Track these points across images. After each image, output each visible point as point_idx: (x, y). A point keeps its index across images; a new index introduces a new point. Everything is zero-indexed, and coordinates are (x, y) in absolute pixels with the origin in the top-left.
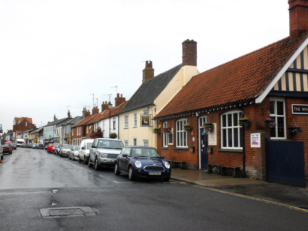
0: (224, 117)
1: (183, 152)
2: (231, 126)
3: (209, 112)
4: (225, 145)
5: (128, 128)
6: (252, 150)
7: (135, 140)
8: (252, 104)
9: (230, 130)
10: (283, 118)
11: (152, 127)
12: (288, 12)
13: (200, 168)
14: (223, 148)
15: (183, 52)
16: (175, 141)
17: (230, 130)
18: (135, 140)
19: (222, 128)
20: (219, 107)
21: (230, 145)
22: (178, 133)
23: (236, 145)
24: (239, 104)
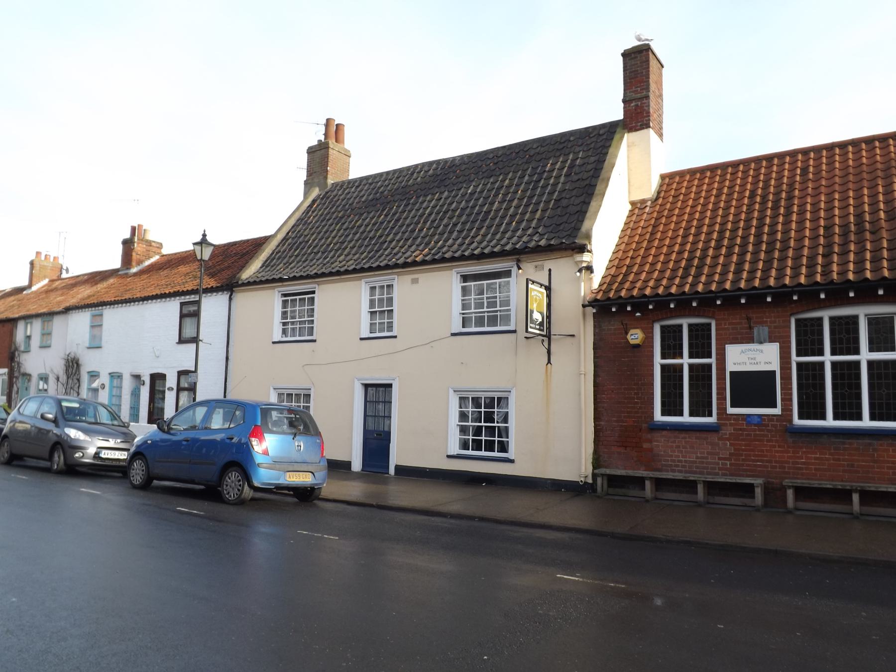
16: (787, 399)
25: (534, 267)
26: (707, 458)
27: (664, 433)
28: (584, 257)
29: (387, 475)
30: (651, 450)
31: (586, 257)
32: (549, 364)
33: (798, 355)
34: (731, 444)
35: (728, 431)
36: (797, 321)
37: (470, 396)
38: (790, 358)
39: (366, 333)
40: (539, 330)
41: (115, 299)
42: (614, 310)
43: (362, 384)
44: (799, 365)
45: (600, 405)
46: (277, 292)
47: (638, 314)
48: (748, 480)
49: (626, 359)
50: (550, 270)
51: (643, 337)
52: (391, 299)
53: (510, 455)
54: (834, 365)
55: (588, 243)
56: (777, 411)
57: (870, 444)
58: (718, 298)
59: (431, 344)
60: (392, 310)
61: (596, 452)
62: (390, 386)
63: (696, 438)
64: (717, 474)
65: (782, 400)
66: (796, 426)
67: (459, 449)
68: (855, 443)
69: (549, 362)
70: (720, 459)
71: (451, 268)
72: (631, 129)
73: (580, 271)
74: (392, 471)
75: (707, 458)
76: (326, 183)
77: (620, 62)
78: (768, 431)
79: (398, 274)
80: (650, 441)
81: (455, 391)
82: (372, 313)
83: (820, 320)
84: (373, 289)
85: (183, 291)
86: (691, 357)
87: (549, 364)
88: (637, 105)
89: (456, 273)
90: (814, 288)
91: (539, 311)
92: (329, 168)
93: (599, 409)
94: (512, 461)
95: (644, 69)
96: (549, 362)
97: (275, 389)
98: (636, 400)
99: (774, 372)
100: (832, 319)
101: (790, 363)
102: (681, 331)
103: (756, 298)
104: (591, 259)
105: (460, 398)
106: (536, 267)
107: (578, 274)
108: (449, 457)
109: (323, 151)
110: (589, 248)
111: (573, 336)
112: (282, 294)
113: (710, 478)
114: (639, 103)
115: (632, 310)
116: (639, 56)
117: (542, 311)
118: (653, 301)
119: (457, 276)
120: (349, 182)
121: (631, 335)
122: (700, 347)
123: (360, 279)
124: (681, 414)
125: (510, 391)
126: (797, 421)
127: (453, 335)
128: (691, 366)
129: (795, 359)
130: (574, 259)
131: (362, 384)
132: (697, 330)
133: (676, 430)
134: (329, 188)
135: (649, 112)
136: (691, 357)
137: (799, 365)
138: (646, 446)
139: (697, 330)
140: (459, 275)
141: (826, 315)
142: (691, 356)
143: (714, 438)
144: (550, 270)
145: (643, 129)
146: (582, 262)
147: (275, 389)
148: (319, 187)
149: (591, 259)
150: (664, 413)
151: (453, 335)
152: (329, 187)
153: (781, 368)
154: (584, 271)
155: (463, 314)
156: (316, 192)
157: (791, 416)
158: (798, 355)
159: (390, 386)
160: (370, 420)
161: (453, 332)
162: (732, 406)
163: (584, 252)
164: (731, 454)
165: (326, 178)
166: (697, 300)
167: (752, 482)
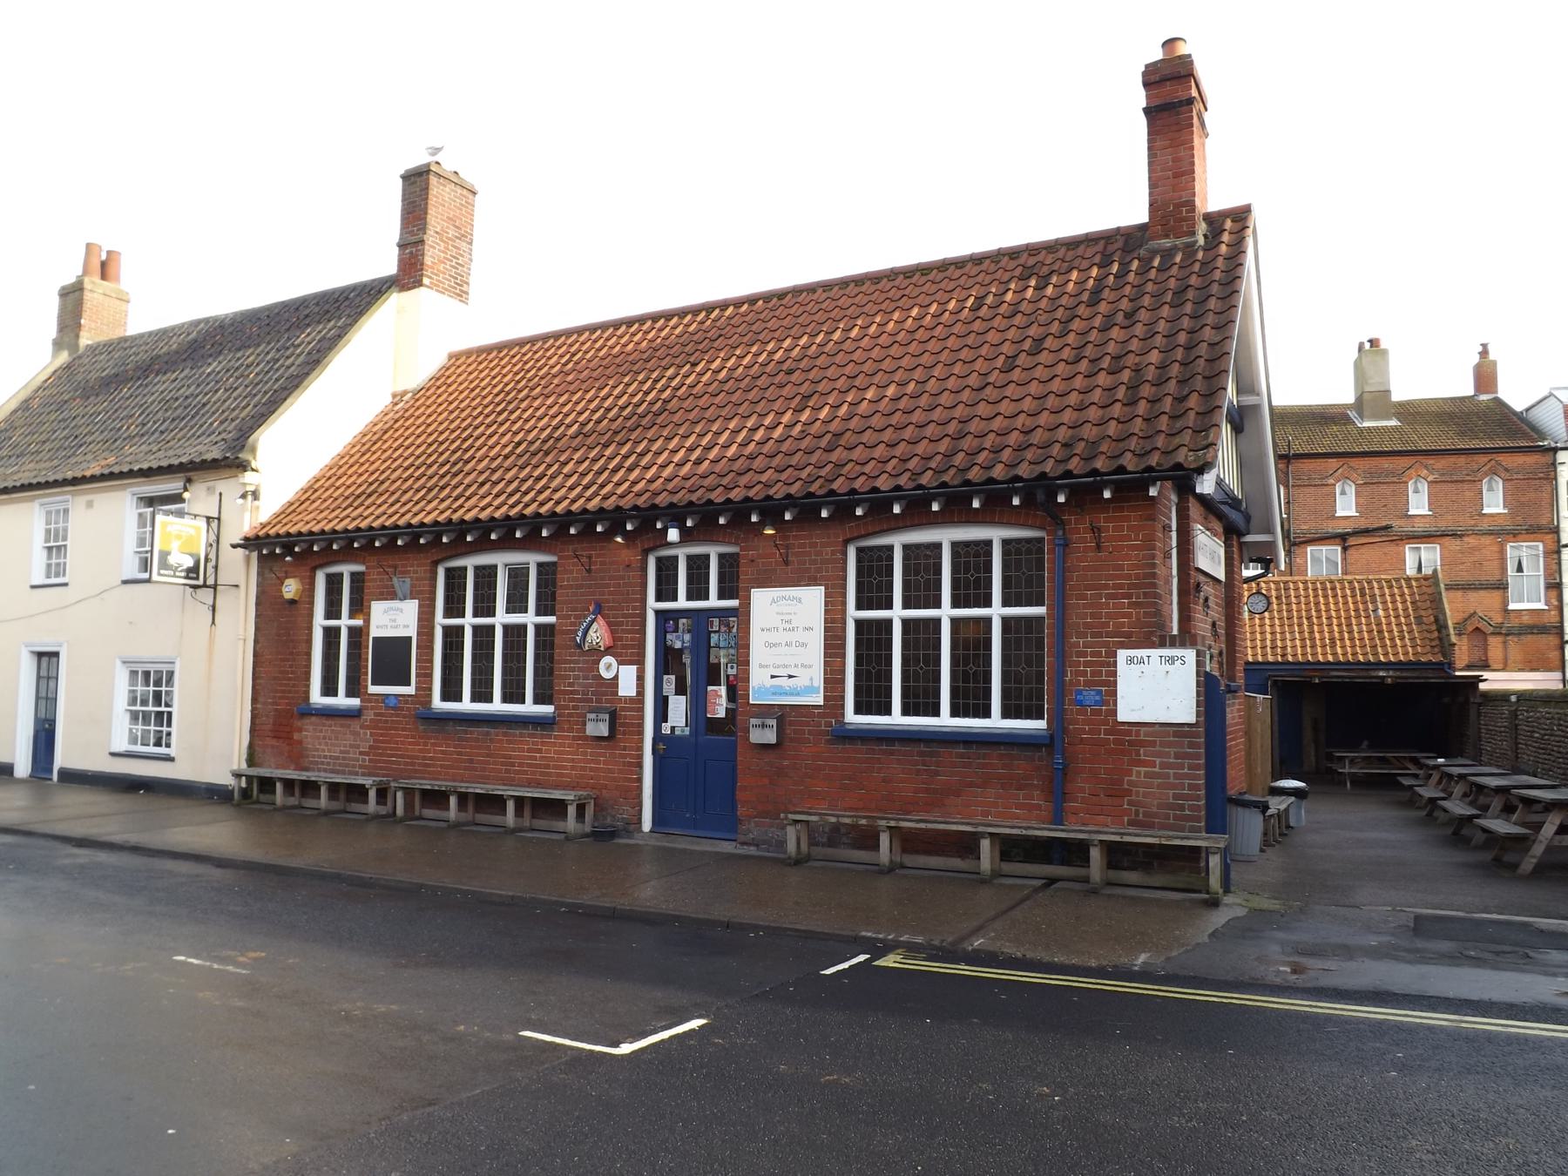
0: (455, 580)
1: (505, 734)
2: (338, 617)
3: (625, 534)
4: (451, 692)
5: (66, 585)
6: (1129, 733)
7: (47, 659)
8: (321, 550)
9: (484, 636)
10: (659, 598)
11: (215, 587)
12: (1142, 123)
13: (647, 825)
14: (438, 704)
15: (402, 224)
16: (426, 675)
17: (484, 636)
18: (47, 659)
19: (440, 620)
20: (272, 543)
21: (921, 700)
22: (331, 635)
23: (971, 700)
24: (419, 536)
26: (348, 752)
27: (314, 719)
29: (49, 782)
30: (300, 742)
31: (248, 477)
33: (859, 607)
34: (371, 734)
35: (369, 716)
36: (860, 551)
37: (140, 669)
38: (844, 612)
39: (41, 580)
42: (824, 514)
43: (33, 652)
44: (860, 624)
46: (130, 496)
47: (769, 532)
48: (557, 795)
50: (221, 494)
51: (297, 590)
52: (65, 530)
53: (172, 752)
54: (906, 623)
56: (410, 690)
57: (488, 734)
58: (934, 498)
60: (65, 546)
61: (251, 746)
62: (56, 654)
63: (342, 726)
64: (356, 774)
65: (418, 675)
66: (851, 727)
67: (129, 743)
68: (477, 731)
69: (213, 623)
70: (361, 753)
71: (124, 487)
72: (405, 287)
73: (244, 496)
74: (55, 777)
75: (348, 752)
76: (77, 345)
77: (397, 186)
78: (404, 716)
79: (73, 494)
80: (300, 730)
82: (50, 549)
83: (890, 548)
84: (49, 513)
86: (906, 606)
88: (411, 253)
90: (706, 508)
91: (188, 551)
92: (83, 321)
94: (172, 759)
95: (422, 200)
96: (213, 623)
97: (124, 662)
99: (410, 638)
100: (906, 548)
101: (433, 628)
102: (989, 554)
103: (806, 508)
106: (208, 489)
107: (241, 501)
108: (113, 754)
109: (77, 293)
110: (254, 465)
111: (237, 586)
113: (338, 779)
114: (414, 250)
115: (1113, 497)
116: (418, 180)
118: (1066, 486)
120: (125, 339)
122: (359, 606)
123: (32, 499)
124: (937, 713)
126: (851, 717)
127: (125, 582)
128: (1006, 621)
129: (853, 613)
132: (460, 577)
133: (323, 715)
134: (80, 352)
135: (422, 264)
136: (906, 606)
137: (860, 624)
138: (296, 736)
139: (1018, 552)
141: (898, 541)
142: (907, 605)
143: (355, 725)
144: (221, 494)
145: (414, 287)
147: (124, 662)
148: (68, 349)
150: (858, 711)
151: (125, 582)
152: (81, 350)
153: (419, 634)
156: (64, 357)
157: (430, 696)
158: (859, 607)
159: (56, 654)
160: (42, 703)
162: (373, 683)
164: (370, 747)
165: (77, 336)
166: (1067, 490)
167: (364, 782)
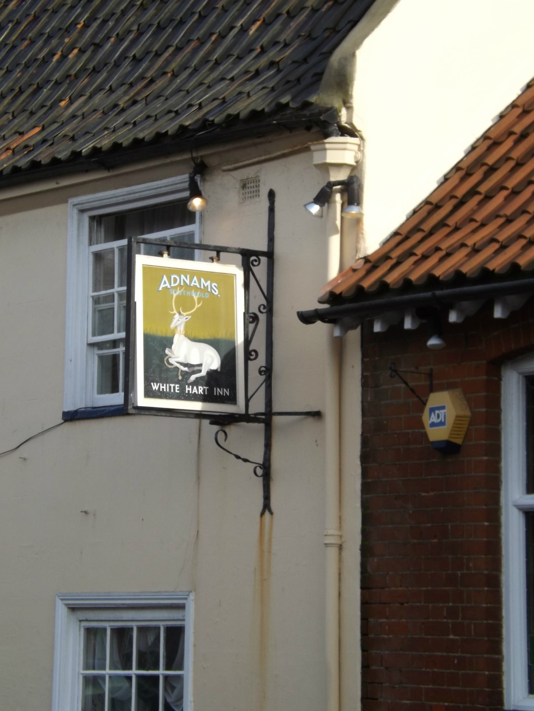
25: (238, 185)
28: (329, 152)
32: (267, 513)
40: (205, 398)
41: (75, 147)
45: (373, 652)
49: (432, 493)
50: (272, 195)
55: (337, 103)
59: (24, 451)
69: (267, 506)
81: (73, 609)
85: (233, 119)
87: (267, 513)
89: (75, 211)
93: (373, 668)
96: (267, 506)
98: (452, 637)
104: (359, 155)
105: (89, 631)
112: (92, 218)
117: (221, 335)
119: (80, 221)
121: (432, 410)
125: (182, 607)
130: (312, 158)
131: (67, 605)
140: (86, 218)
144: (272, 195)
146: (326, 167)
149: (359, 155)
154: (338, 197)
155: (99, 345)
161: (70, 408)
163: (327, 135)
